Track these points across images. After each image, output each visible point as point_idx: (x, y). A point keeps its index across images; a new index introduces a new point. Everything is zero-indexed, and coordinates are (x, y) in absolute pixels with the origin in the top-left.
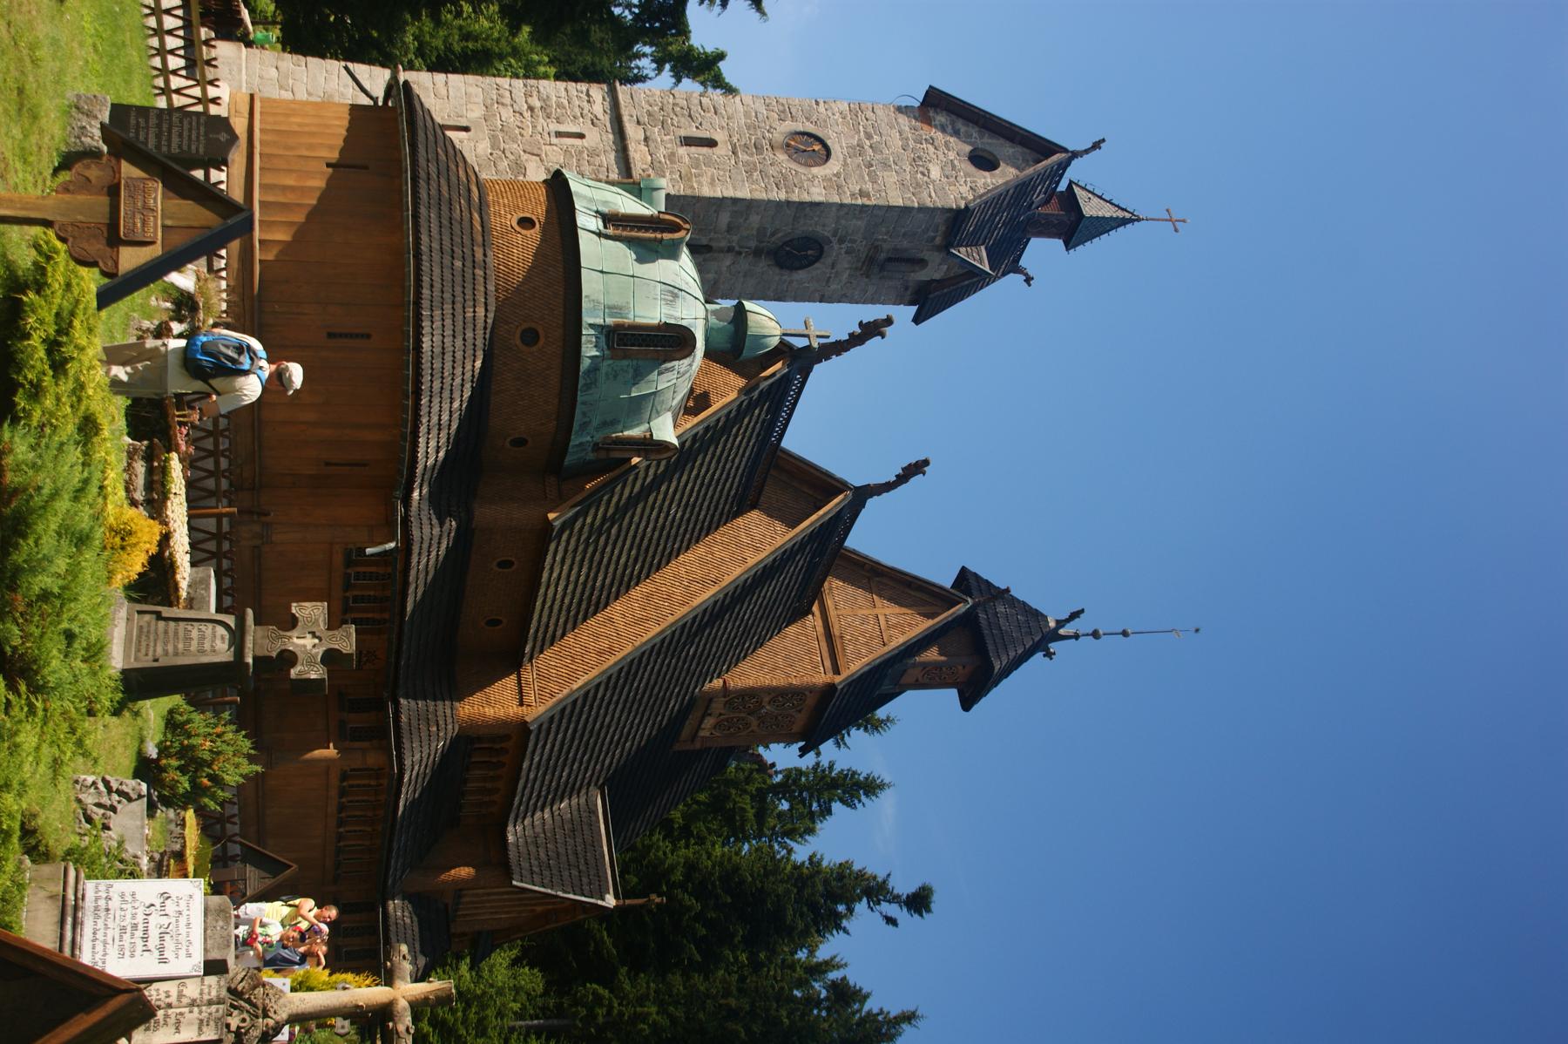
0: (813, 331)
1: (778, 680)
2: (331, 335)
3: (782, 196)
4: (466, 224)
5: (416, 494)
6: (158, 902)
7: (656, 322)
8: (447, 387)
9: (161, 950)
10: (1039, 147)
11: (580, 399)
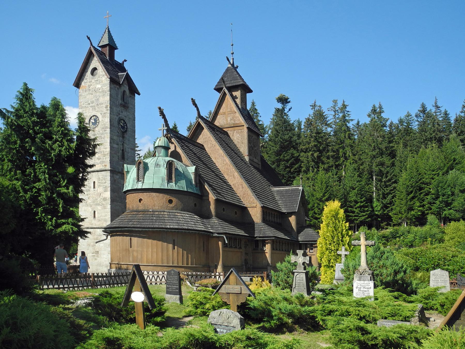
0: (162, 128)
1: (246, 141)
5: (211, 231)
7: (165, 170)
9: (368, 288)
10: (90, 56)
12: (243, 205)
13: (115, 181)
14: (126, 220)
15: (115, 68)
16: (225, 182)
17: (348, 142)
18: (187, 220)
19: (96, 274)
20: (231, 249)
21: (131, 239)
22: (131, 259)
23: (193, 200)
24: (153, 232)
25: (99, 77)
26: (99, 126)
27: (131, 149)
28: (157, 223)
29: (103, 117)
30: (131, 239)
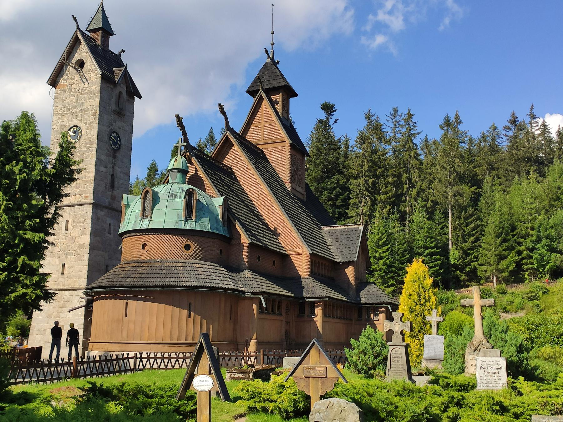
5: (243, 289)
8: (208, 277)
9: (498, 369)
10: (75, 43)
12: (284, 252)
13: (98, 219)
14: (122, 276)
15: (109, 61)
16: (259, 218)
17: (413, 162)
18: (209, 274)
19: (109, 358)
20: (268, 317)
21: (127, 303)
22: (125, 334)
23: (219, 245)
24: (161, 292)
26: (81, 141)
27: (124, 173)
30: (127, 303)
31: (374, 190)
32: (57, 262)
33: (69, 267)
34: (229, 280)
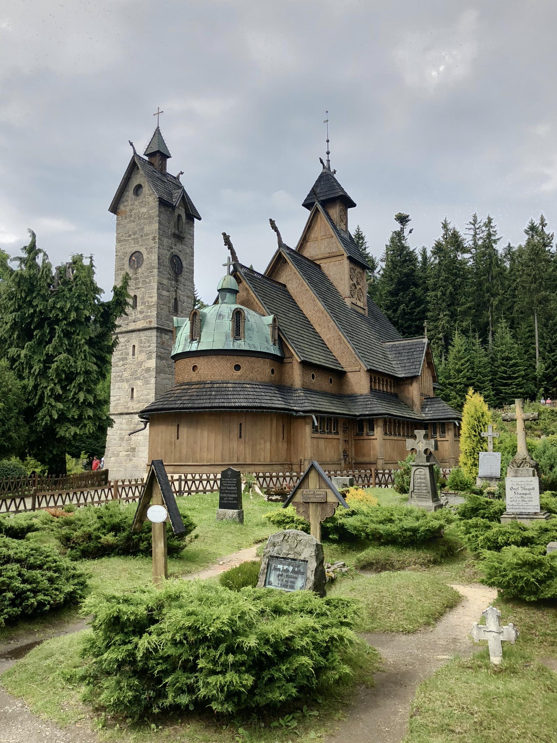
2: (240, 437)
3: (156, 271)
4: (198, 390)
6: (514, 491)
9: (529, 489)
10: (133, 167)
11: (259, 350)
12: (340, 369)
18: (260, 394)
20: (322, 436)
25: (145, 197)
26: (143, 266)
28: (217, 401)
29: (148, 253)
31: (453, 302)
32: (127, 388)
33: (137, 391)
34: (280, 399)
